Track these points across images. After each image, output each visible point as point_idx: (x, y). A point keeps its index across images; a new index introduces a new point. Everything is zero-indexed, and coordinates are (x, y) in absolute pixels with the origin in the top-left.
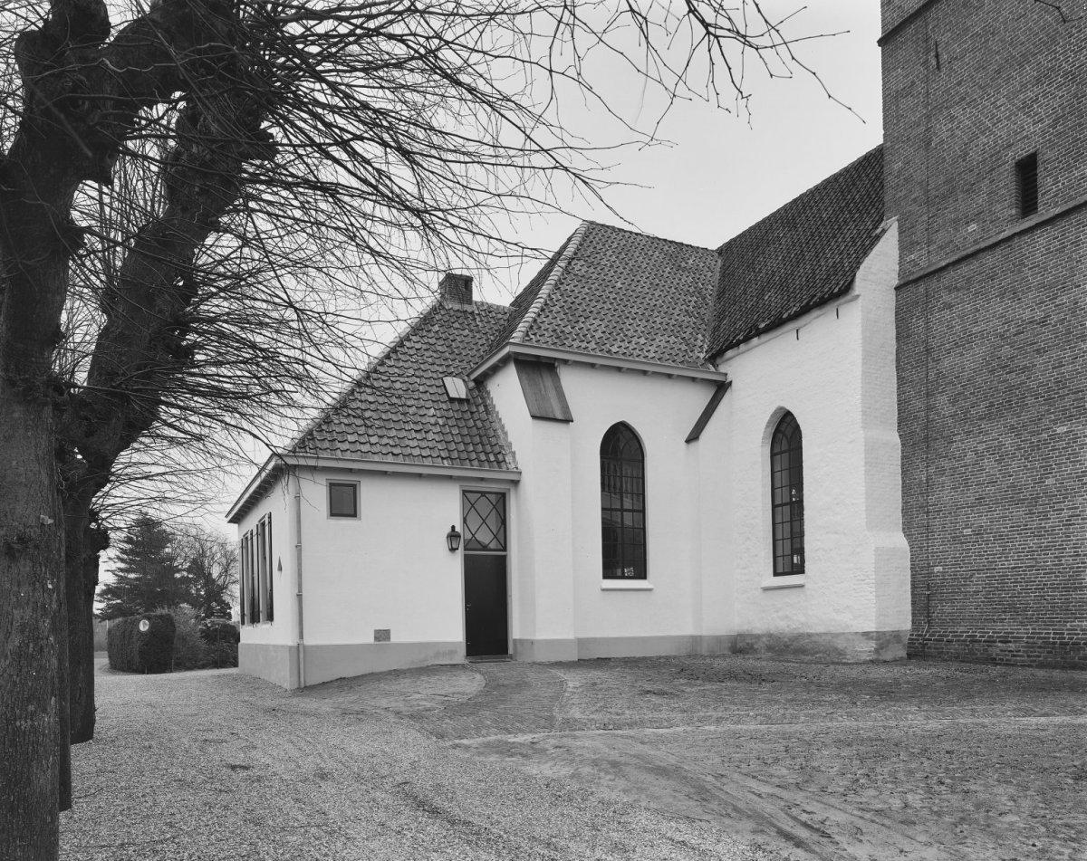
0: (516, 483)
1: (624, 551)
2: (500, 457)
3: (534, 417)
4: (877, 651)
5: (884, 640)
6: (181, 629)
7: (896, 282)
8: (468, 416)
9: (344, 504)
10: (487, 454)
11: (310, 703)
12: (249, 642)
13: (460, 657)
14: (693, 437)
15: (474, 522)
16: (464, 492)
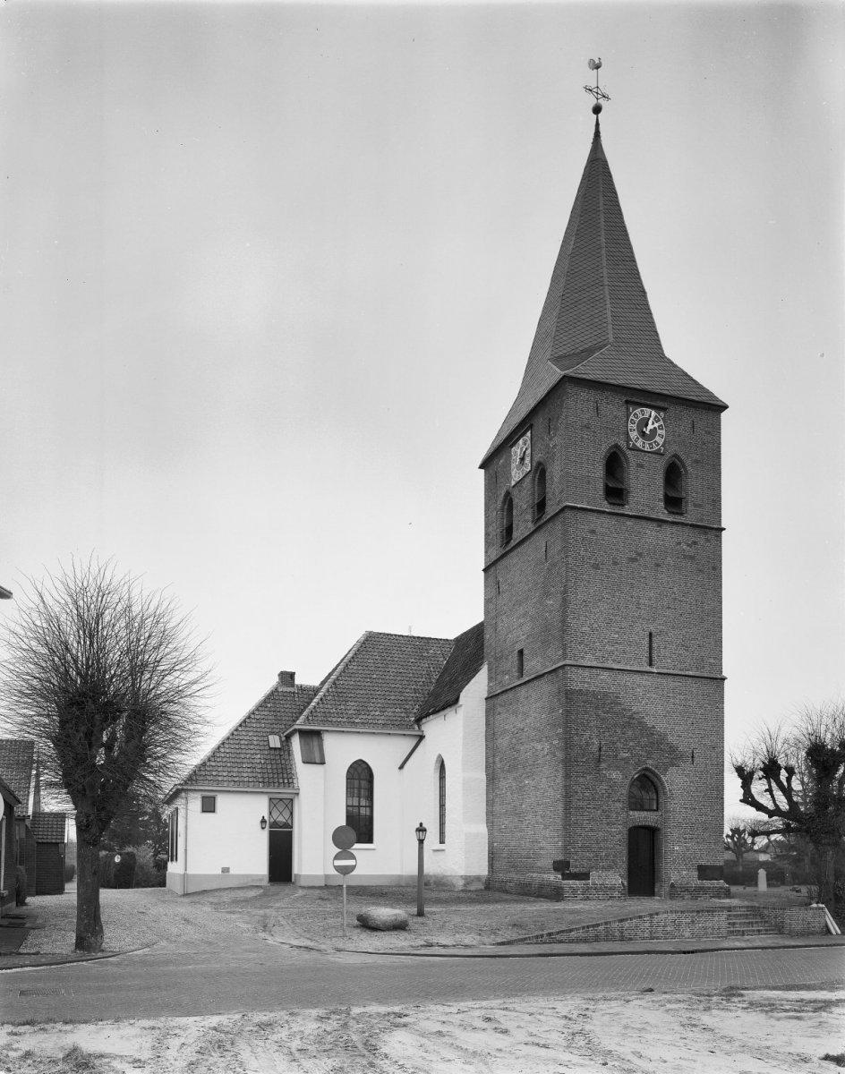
0: (298, 794)
1: (359, 827)
2: (290, 781)
3: (304, 762)
4: (465, 885)
5: (469, 880)
6: (141, 861)
7: (486, 696)
8: (278, 757)
9: (209, 806)
10: (283, 778)
12: (237, 873)
13: (265, 882)
14: (401, 767)
15: (275, 814)
16: (270, 799)
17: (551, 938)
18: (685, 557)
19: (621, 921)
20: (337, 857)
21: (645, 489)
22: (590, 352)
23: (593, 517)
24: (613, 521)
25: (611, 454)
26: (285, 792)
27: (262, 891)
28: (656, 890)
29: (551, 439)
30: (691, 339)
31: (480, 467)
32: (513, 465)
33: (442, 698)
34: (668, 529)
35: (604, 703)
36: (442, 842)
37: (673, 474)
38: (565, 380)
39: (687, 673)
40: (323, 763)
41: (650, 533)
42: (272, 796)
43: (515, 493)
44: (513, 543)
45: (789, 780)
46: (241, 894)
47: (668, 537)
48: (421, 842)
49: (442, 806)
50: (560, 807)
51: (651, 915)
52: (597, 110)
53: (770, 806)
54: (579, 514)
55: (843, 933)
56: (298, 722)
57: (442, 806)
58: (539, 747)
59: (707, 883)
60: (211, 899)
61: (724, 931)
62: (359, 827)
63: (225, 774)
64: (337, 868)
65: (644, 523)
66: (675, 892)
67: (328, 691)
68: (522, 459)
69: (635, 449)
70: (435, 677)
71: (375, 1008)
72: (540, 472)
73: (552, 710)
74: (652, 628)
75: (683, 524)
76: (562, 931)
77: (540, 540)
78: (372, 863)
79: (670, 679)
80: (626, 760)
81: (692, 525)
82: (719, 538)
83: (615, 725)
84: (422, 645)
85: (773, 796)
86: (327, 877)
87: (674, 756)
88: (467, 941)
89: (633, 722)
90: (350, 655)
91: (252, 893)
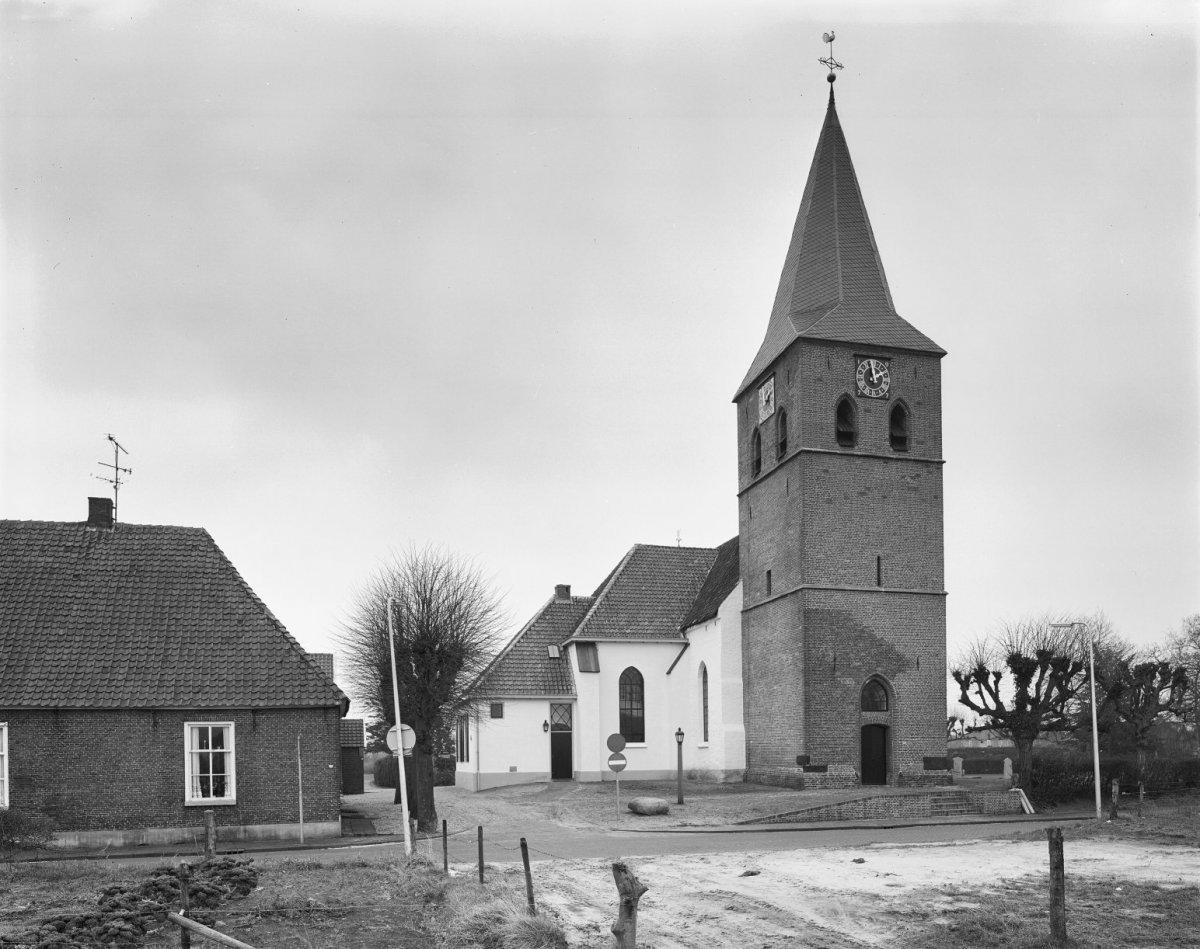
0: (576, 699)
1: (632, 728)
5: (729, 774)
7: (741, 609)
11: (477, 795)
13: (549, 779)
14: (669, 673)
17: (782, 819)
18: (909, 489)
19: (839, 804)
20: (611, 758)
21: (873, 430)
22: (822, 309)
23: (827, 459)
24: (844, 461)
25: (846, 400)
26: (564, 698)
27: (546, 787)
28: (887, 779)
29: (789, 389)
30: (916, 297)
31: (734, 402)
32: (760, 406)
33: (703, 612)
34: (893, 465)
35: (838, 620)
36: (706, 740)
37: (898, 416)
38: (800, 340)
39: (912, 590)
40: (598, 671)
41: (878, 470)
42: (553, 702)
43: (762, 430)
44: (761, 475)
45: (996, 683)
46: (529, 790)
47: (893, 472)
48: (680, 743)
49: (706, 707)
50: (801, 710)
51: (865, 800)
52: (831, 79)
53: (982, 707)
54: (814, 457)
55: (1037, 812)
56: (575, 634)
57: (706, 707)
58: (784, 657)
59: (932, 773)
60: (504, 795)
61: (928, 812)
62: (632, 728)
63: (510, 683)
64: (611, 767)
65: (872, 461)
66: (903, 781)
67: (601, 604)
68: (768, 401)
69: (863, 396)
70: (700, 586)
71: (635, 857)
72: (782, 415)
73: (794, 626)
74: (880, 553)
75: (907, 460)
76: (790, 814)
77: (782, 475)
78: (642, 760)
79: (897, 597)
80: (858, 669)
81: (914, 460)
82: (940, 469)
83: (849, 638)
84: (686, 556)
85: (983, 698)
86: (603, 773)
87: (901, 664)
88: (714, 822)
89: (863, 635)
90: (621, 568)
91: (539, 789)
